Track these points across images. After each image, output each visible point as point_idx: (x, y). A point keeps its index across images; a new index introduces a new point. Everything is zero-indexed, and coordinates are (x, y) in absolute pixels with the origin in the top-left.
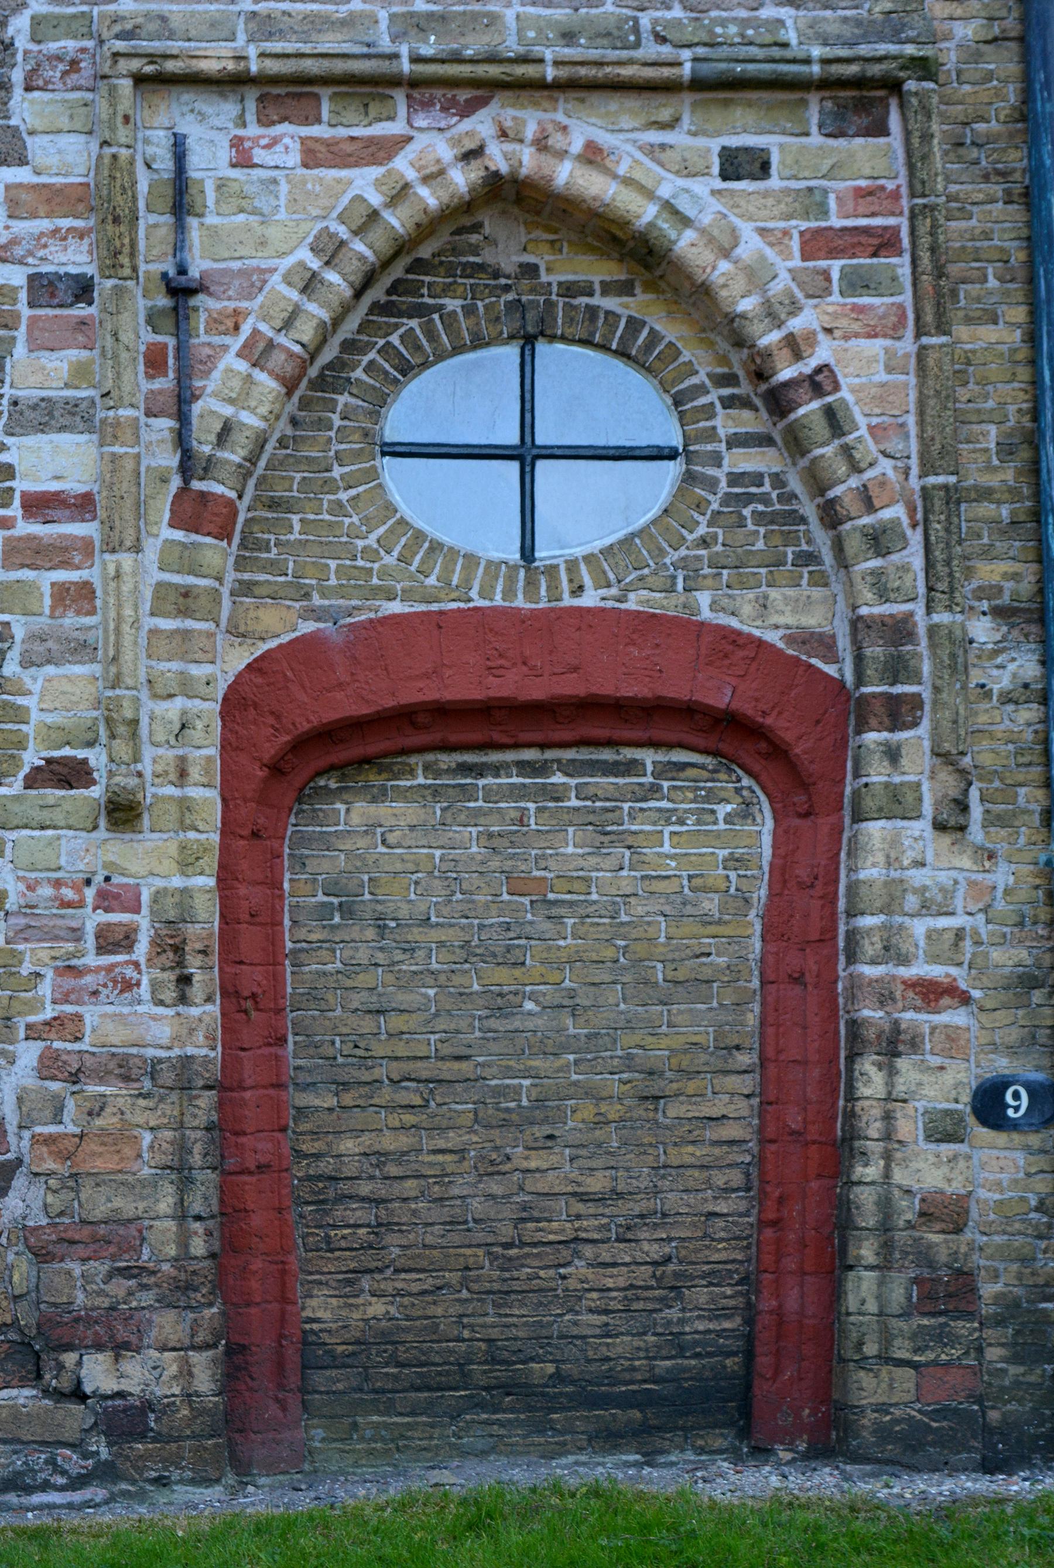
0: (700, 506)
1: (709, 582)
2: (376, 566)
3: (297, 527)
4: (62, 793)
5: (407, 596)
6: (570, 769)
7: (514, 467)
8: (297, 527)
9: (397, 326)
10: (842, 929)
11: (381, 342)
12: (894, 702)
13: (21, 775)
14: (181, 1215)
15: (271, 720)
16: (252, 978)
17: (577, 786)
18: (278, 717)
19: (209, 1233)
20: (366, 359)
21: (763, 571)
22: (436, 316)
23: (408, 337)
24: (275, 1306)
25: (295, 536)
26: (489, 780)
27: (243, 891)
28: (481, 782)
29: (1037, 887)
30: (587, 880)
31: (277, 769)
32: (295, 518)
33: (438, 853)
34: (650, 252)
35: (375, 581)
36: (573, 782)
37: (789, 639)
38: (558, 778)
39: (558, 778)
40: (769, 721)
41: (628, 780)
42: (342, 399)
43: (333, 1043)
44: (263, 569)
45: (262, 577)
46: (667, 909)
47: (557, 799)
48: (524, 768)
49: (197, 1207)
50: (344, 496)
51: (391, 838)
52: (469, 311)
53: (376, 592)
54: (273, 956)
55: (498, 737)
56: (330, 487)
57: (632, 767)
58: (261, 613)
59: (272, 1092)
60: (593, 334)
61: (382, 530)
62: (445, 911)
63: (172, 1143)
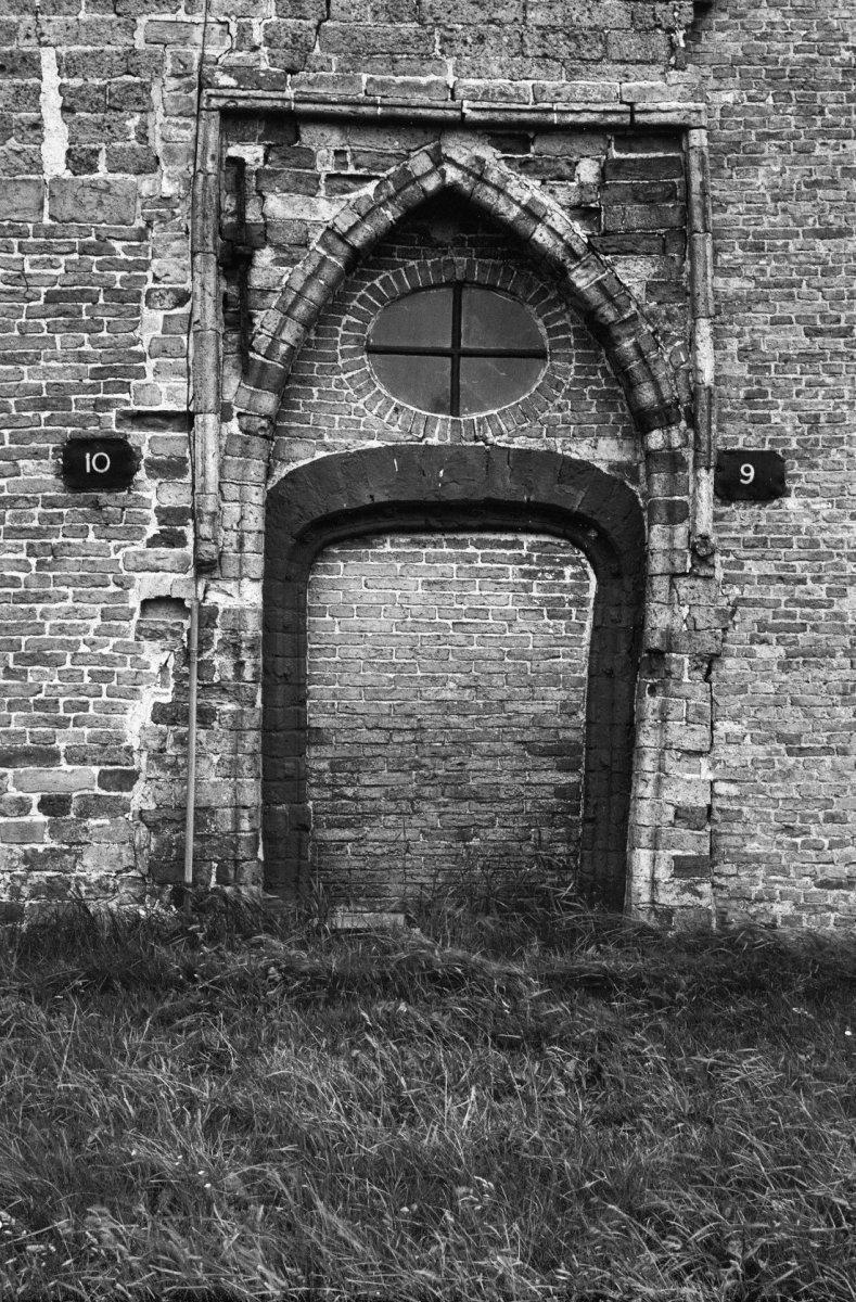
0: (559, 385)
1: (562, 432)
2: (363, 419)
3: (316, 395)
4: (170, 550)
5: (380, 437)
6: (479, 544)
7: (449, 360)
8: (316, 395)
9: (379, 274)
10: (467, 536)
11: (369, 284)
12: (671, 506)
13: (145, 539)
14: (238, 807)
15: (297, 510)
16: (284, 665)
17: (482, 555)
18: (302, 508)
19: (251, 817)
20: (359, 294)
21: (595, 426)
22: (402, 269)
23: (384, 283)
24: (295, 861)
25: (315, 400)
26: (430, 550)
27: (279, 612)
28: (424, 551)
29: (704, 739)
30: (487, 611)
31: (301, 540)
32: (314, 390)
33: (398, 593)
34: (818, 943)
35: (362, 429)
36: (479, 552)
37: (611, 468)
38: (471, 550)
39: (471, 550)
40: (595, 517)
41: (511, 552)
42: (346, 319)
43: (333, 704)
44: (295, 420)
45: (294, 424)
46: (533, 629)
47: (470, 562)
48: (451, 543)
49: (562, 734)
50: (344, 377)
51: (370, 583)
52: (422, 266)
53: (361, 435)
54: (299, 651)
55: (434, 522)
56: (335, 370)
57: (516, 544)
58: (293, 446)
59: (295, 732)
60: (495, 281)
61: (366, 398)
62: (403, 627)
63: (230, 762)
